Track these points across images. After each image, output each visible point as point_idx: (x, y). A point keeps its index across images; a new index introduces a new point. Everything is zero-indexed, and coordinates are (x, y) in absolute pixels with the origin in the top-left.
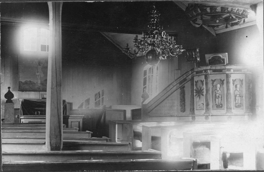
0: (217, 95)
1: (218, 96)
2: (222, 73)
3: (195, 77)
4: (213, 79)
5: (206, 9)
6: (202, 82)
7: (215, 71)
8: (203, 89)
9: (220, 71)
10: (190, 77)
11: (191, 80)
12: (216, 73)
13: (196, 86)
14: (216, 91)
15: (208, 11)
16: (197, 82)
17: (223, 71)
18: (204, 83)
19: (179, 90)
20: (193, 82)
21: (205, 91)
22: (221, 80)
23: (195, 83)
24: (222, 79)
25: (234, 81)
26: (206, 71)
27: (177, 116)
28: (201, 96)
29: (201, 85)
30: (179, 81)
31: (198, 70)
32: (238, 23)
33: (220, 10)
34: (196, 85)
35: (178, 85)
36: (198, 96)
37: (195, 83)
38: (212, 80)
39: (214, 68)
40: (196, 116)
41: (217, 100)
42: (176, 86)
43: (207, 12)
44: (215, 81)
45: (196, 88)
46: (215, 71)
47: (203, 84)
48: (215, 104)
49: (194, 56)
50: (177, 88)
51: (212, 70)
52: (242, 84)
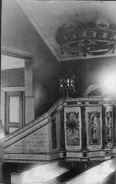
0: (95, 129)
1: (96, 130)
2: (98, 105)
3: (65, 108)
4: (90, 112)
5: (93, 33)
6: (77, 115)
7: (91, 103)
8: (78, 122)
9: (96, 103)
10: (60, 107)
11: (60, 112)
12: (93, 105)
13: (67, 118)
14: (93, 125)
15: (94, 35)
16: (68, 114)
17: (99, 103)
18: (101, 115)
19: (50, 124)
20: (63, 114)
21: (80, 124)
22: (97, 113)
23: (65, 115)
24: (98, 112)
25: (90, 114)
26: (83, 102)
27: (50, 153)
28: (75, 130)
29: (75, 118)
30: (50, 113)
31: (71, 101)
32: (104, 53)
33: (106, 37)
34: (67, 117)
35: (50, 117)
36: (70, 130)
37: (65, 115)
38: (88, 112)
39: (91, 99)
40: (67, 152)
41: (94, 134)
42: (47, 118)
43: (93, 36)
44: (91, 114)
45: (67, 121)
46: (69, 103)
47: (77, 117)
48: (91, 138)
49: (68, 85)
50: (49, 120)
51: (88, 102)
52: (99, 116)
